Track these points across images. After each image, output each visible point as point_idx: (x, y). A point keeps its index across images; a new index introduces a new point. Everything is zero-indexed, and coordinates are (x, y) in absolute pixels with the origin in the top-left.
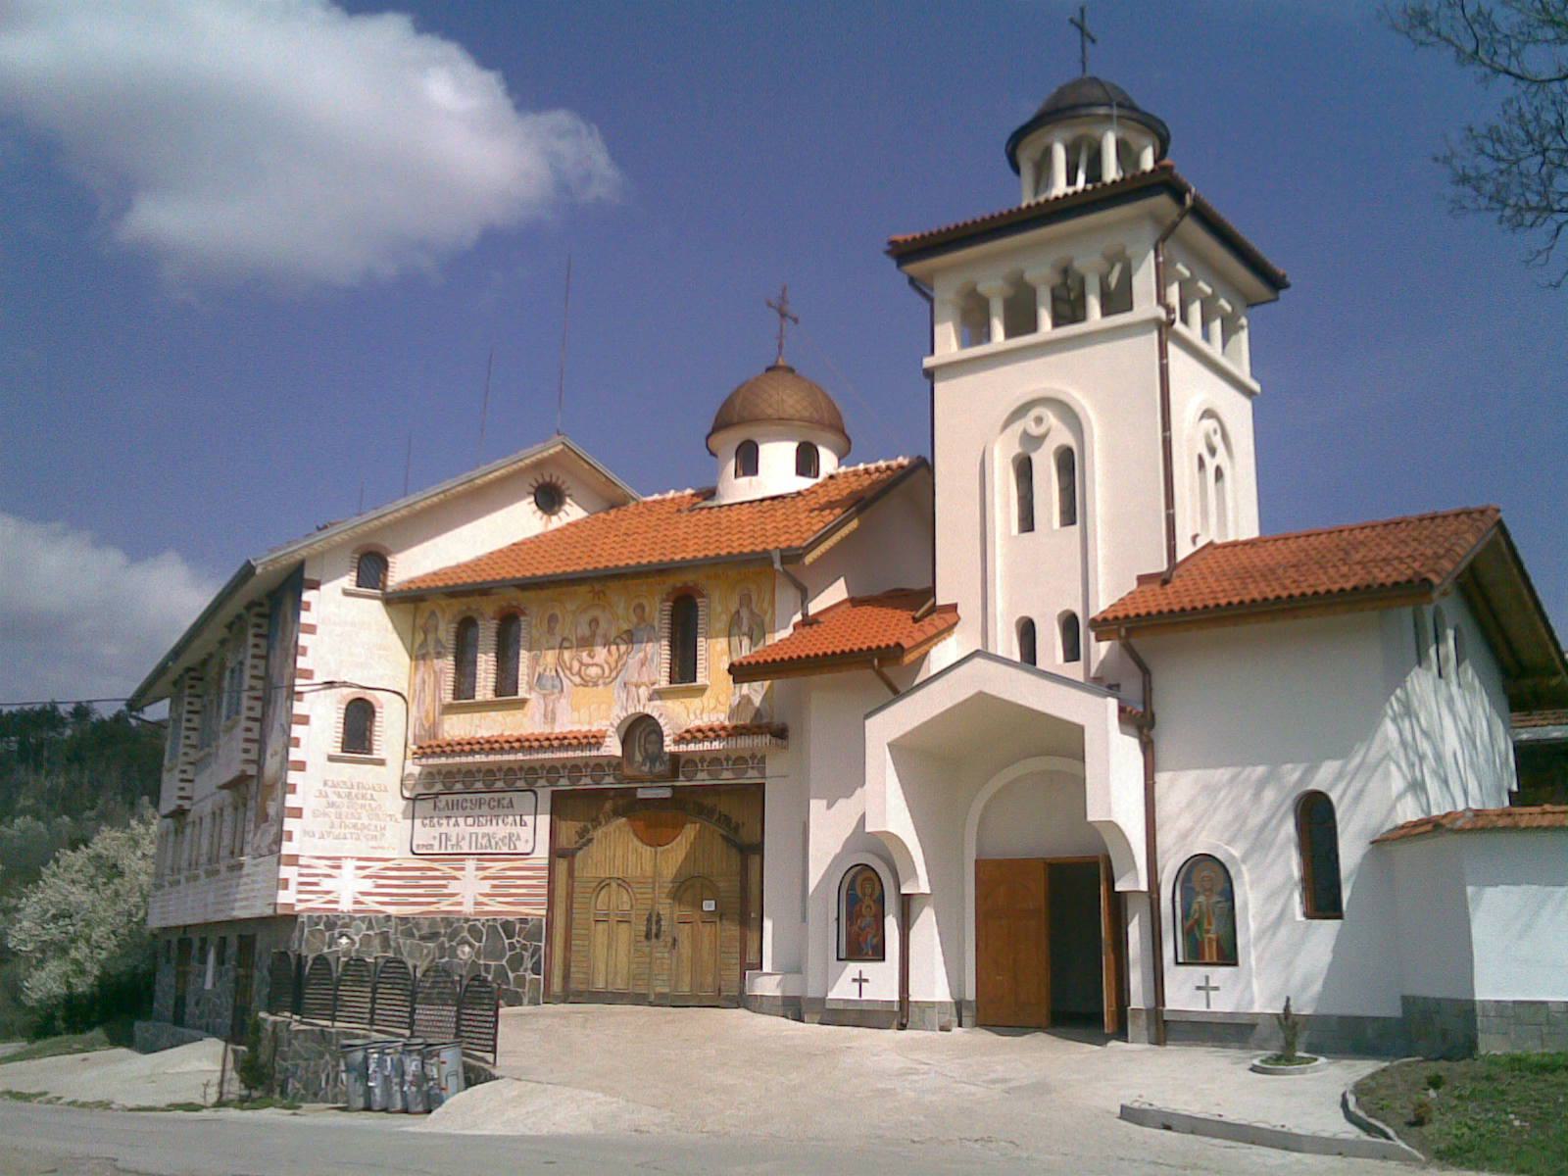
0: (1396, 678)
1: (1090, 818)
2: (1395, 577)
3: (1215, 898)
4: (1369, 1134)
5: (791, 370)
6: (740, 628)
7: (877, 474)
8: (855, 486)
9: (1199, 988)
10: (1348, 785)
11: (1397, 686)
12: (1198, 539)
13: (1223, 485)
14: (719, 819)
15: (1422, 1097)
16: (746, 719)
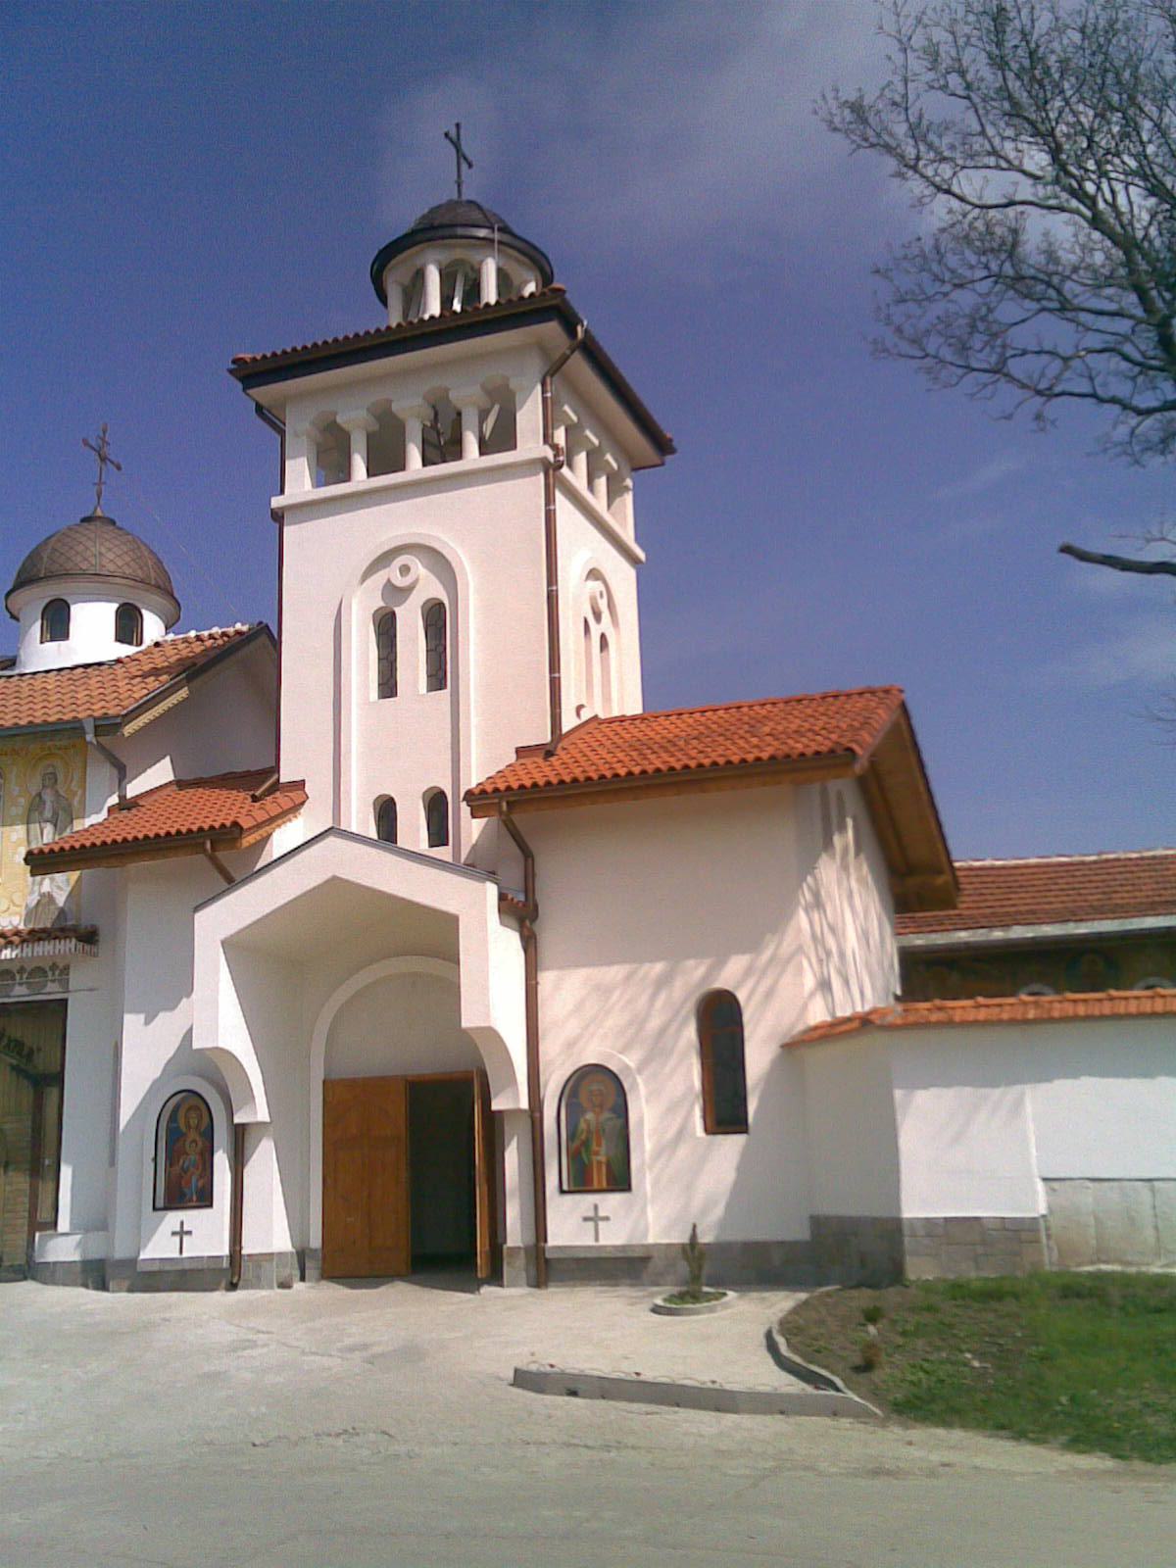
0: (809, 866)
1: (464, 1024)
2: (814, 747)
3: (607, 1115)
4: (817, 1388)
5: (113, 522)
6: (41, 813)
7: (212, 641)
8: (185, 653)
9: (586, 1219)
10: (758, 983)
11: (802, 881)
12: (582, 712)
13: (608, 654)
14: (8, 1045)
15: (862, 1334)
16: (46, 922)
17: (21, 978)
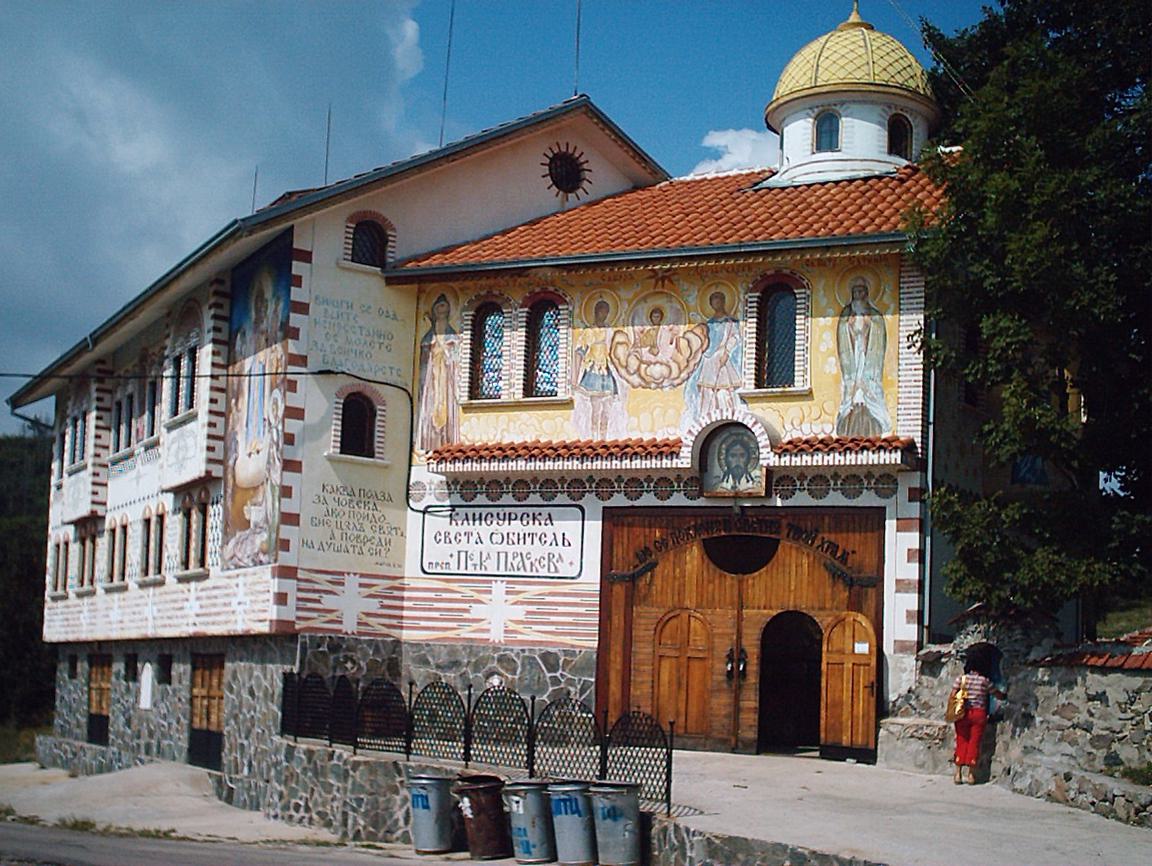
14: (822, 545)
17: (869, 483)
